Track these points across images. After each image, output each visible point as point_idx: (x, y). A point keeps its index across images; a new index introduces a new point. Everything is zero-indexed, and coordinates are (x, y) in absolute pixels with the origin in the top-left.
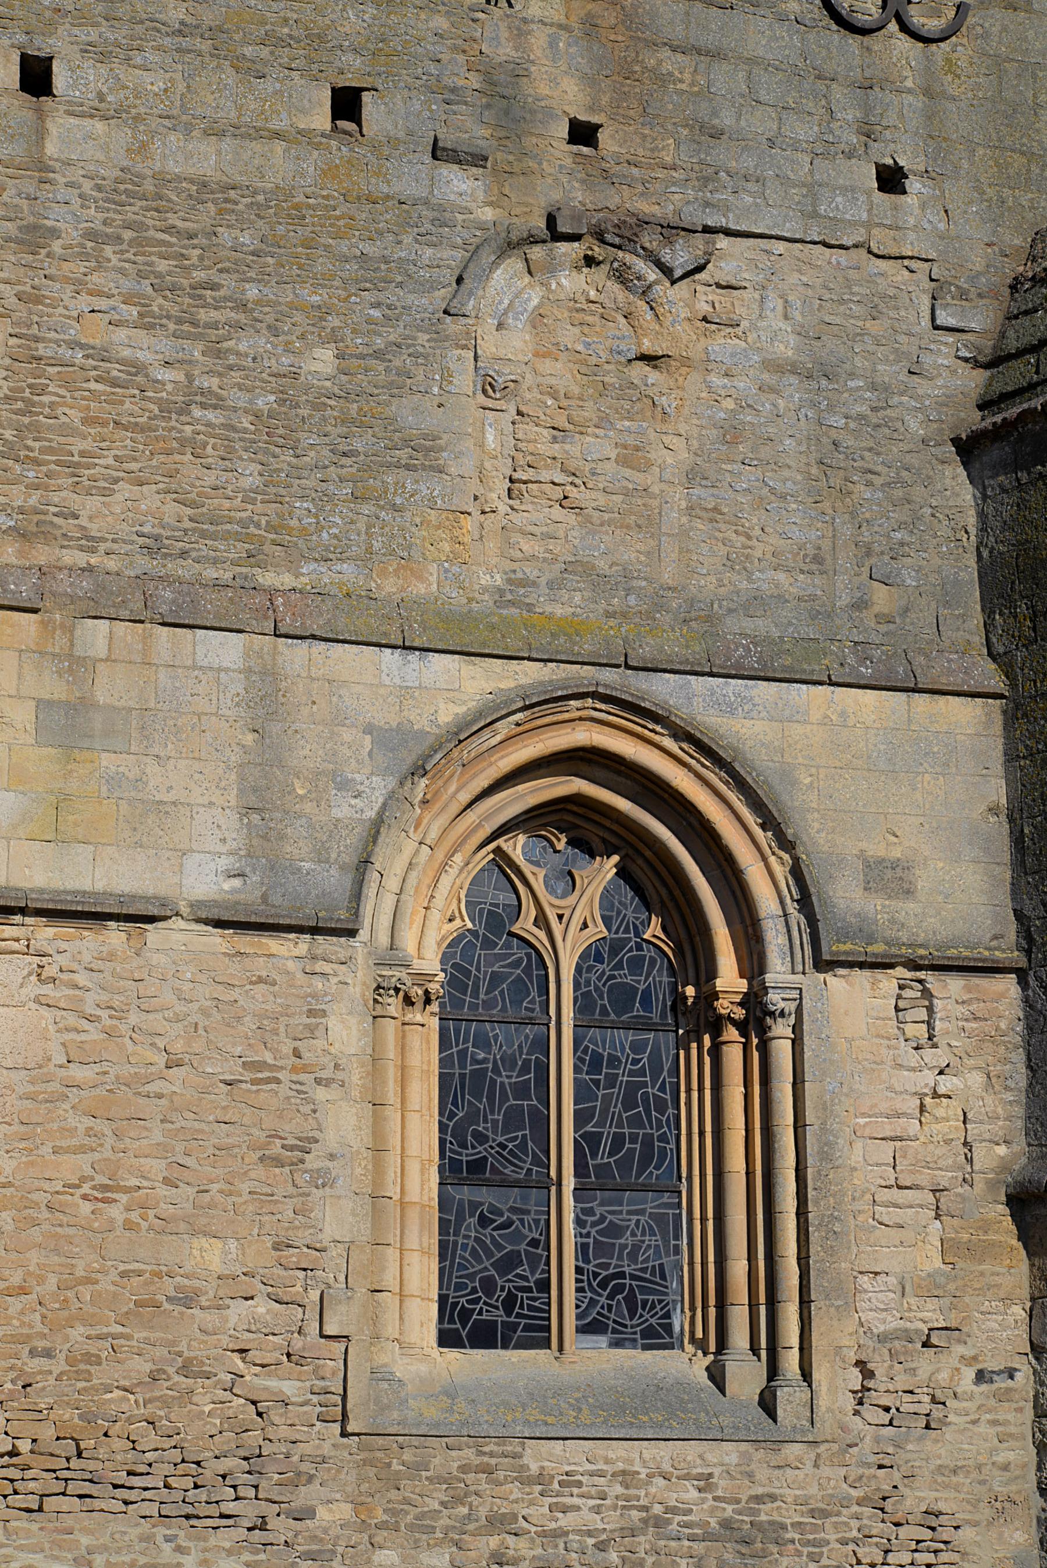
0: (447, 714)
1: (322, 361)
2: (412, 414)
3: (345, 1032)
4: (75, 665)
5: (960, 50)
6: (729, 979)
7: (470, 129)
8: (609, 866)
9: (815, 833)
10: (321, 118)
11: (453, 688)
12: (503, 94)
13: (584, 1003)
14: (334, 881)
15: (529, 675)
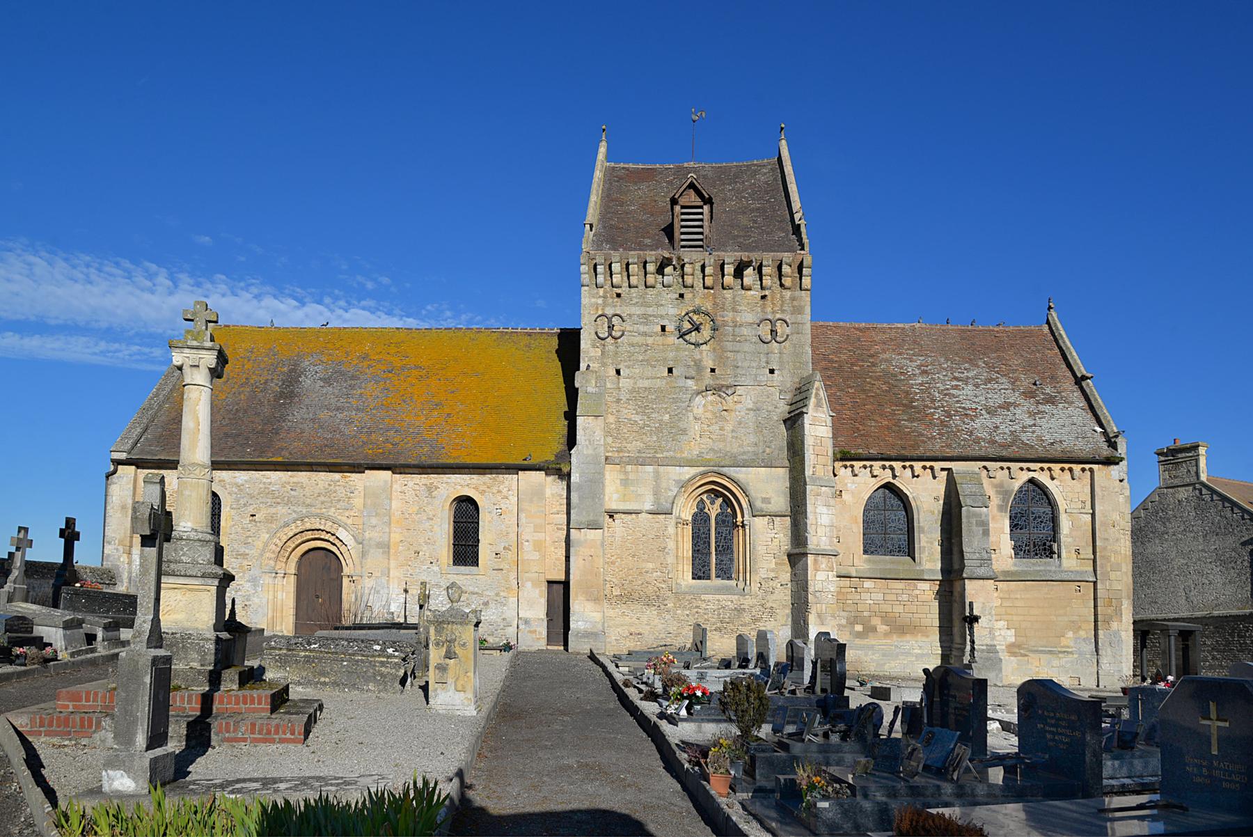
0: (688, 477)
1: (667, 416)
2: (681, 425)
3: (671, 530)
4: (626, 473)
5: (787, 344)
6: (739, 518)
7: (693, 373)
8: (721, 500)
9: (753, 493)
10: (666, 373)
11: (689, 472)
12: (698, 365)
13: (717, 523)
14: (669, 506)
15: (702, 469)
